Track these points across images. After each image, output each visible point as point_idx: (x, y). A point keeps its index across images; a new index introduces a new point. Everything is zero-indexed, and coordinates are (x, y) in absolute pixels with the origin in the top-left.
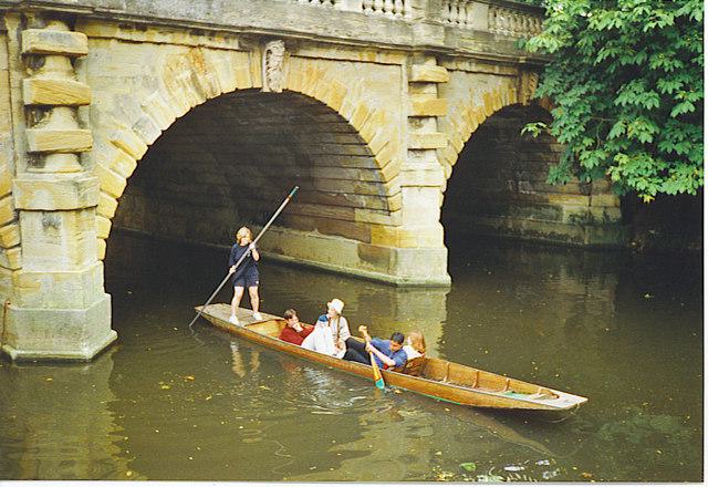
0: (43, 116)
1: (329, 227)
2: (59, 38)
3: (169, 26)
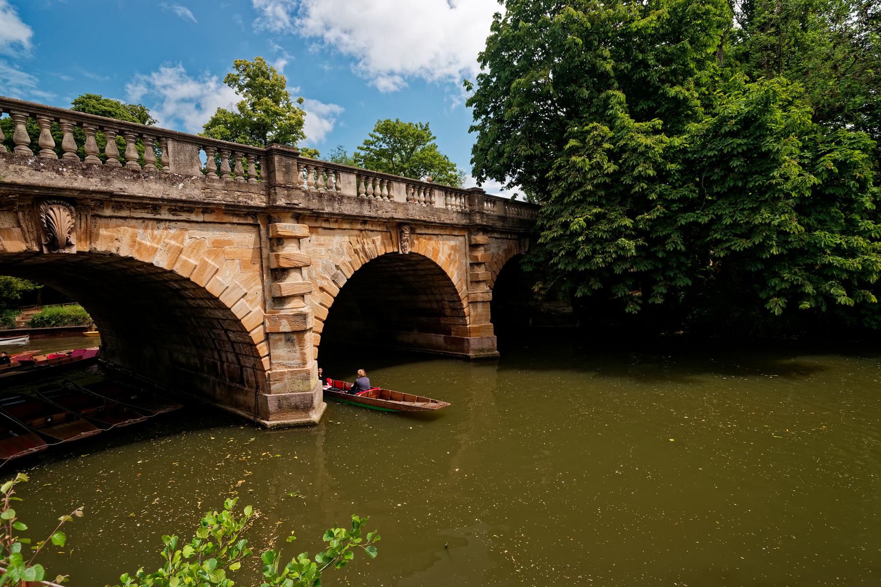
1: (425, 329)
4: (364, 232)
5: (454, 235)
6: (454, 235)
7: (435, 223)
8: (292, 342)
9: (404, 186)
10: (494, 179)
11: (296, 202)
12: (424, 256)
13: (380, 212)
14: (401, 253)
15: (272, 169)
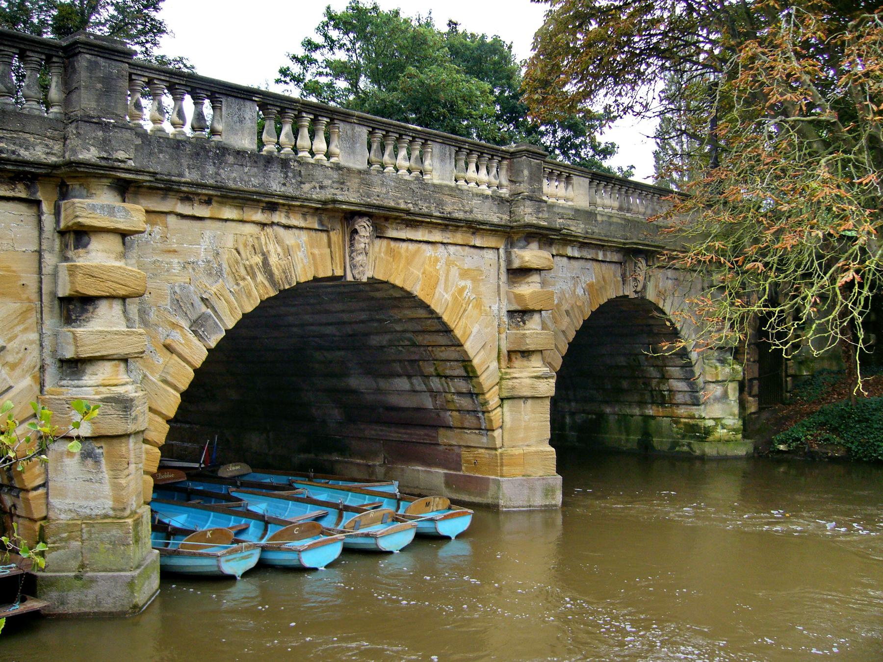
0: (85, 311)
2: (111, 210)
3: (242, 199)
4: (269, 230)
5: (474, 247)
6: (474, 247)
7: (431, 216)
8: (97, 462)
9: (364, 131)
10: (489, 40)
11: (121, 155)
12: (402, 289)
13: (306, 187)
14: (349, 278)
15: (75, 85)
